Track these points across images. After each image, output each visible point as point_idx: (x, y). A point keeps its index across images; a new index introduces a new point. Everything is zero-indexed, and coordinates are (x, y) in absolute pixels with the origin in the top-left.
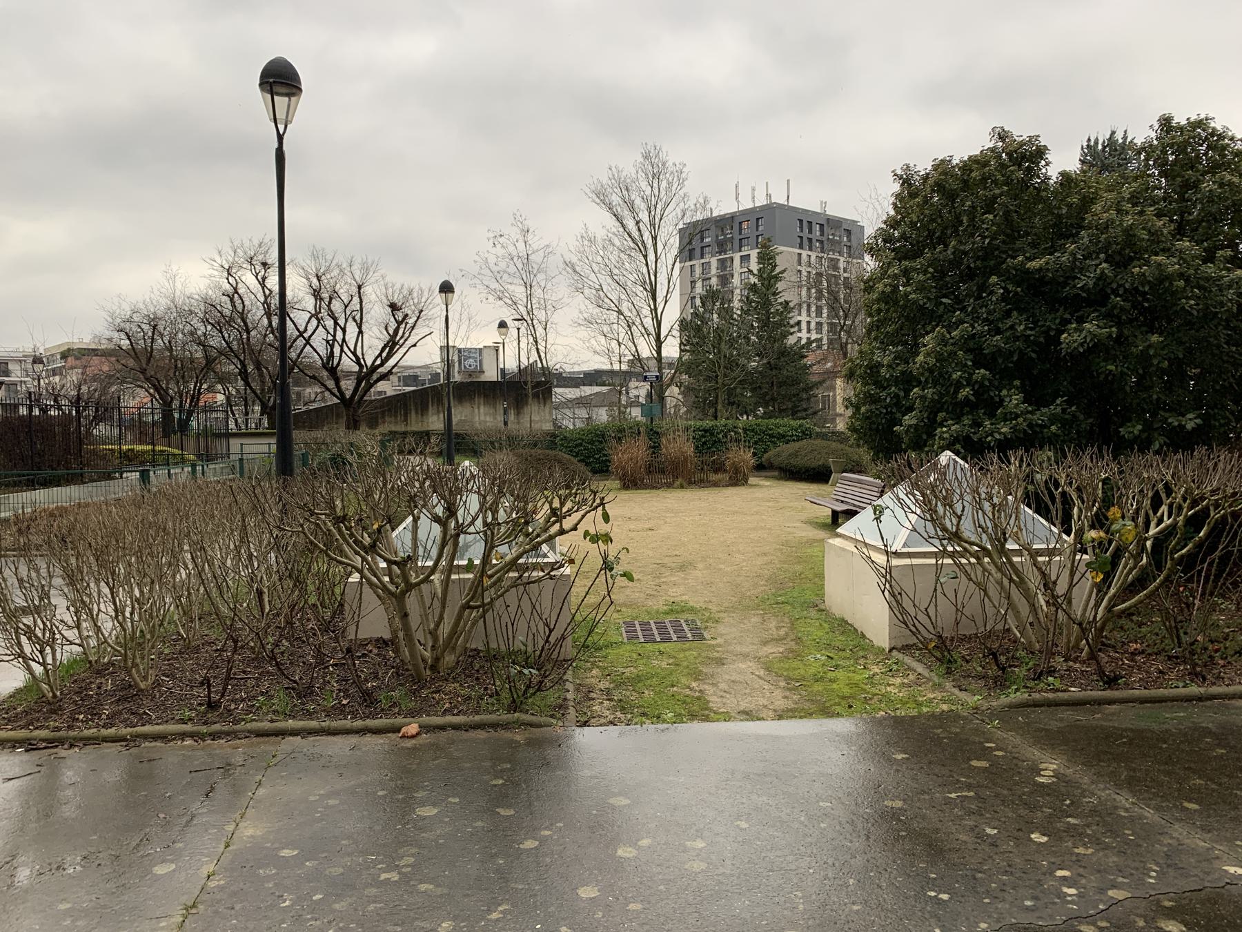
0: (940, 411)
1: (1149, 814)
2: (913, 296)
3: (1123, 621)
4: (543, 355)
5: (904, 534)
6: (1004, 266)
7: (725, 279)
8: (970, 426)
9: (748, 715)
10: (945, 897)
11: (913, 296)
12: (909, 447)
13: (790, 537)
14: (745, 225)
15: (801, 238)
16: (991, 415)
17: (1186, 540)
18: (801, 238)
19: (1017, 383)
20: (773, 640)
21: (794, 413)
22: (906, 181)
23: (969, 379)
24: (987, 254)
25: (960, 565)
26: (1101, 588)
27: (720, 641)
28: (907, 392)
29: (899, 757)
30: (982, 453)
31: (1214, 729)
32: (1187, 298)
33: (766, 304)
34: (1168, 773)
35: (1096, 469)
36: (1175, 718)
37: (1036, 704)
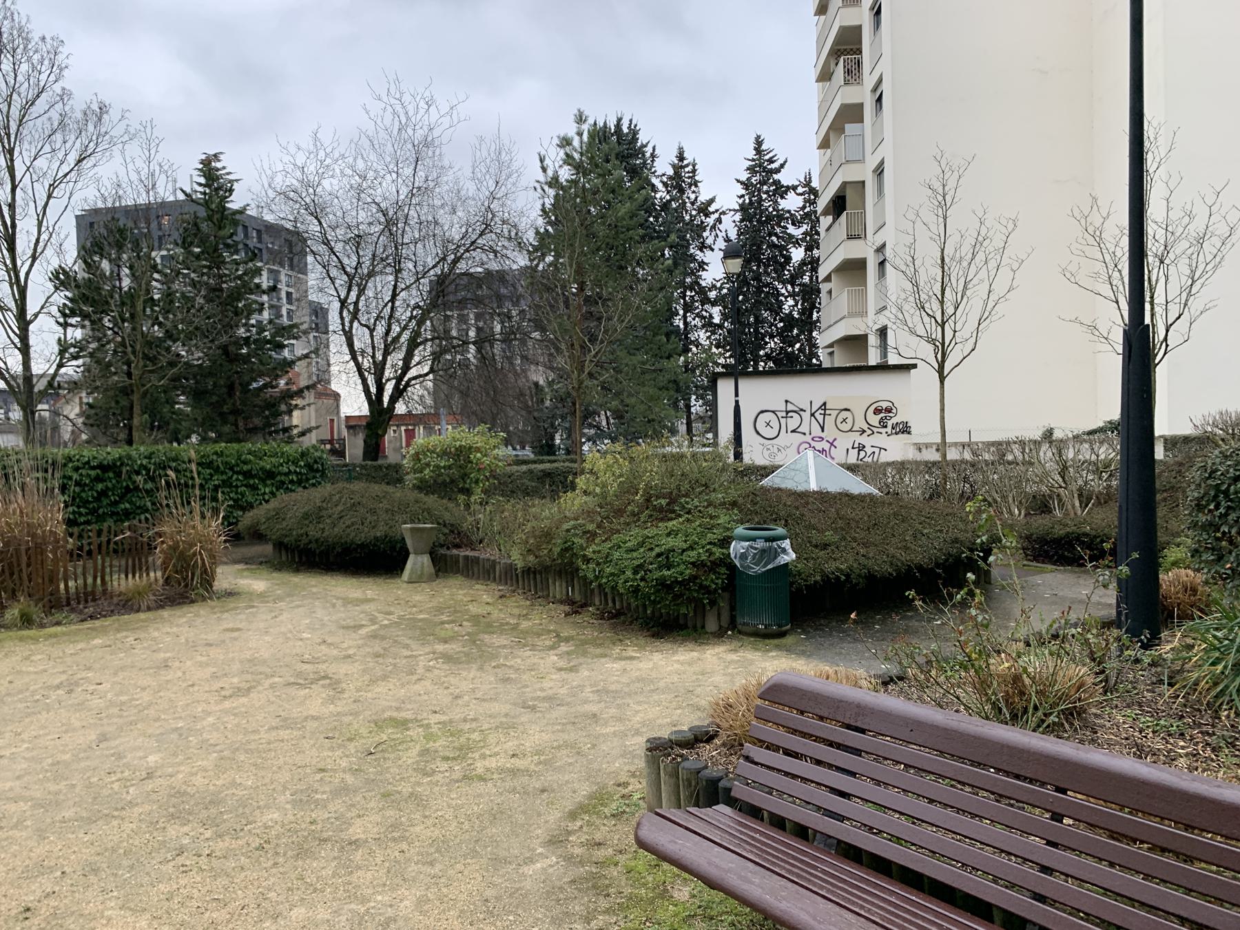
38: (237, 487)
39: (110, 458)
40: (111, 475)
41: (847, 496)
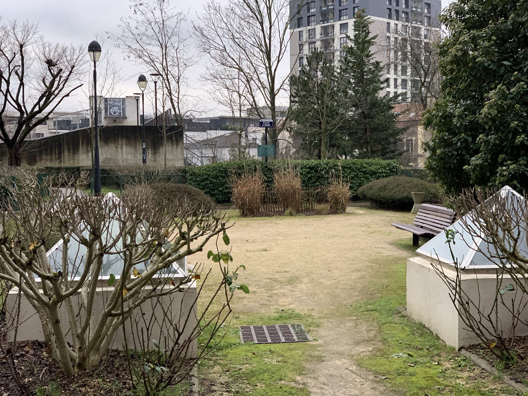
4: (176, 105)
5: (471, 254)
7: (327, 43)
11: (479, 59)
13: (379, 256)
15: (390, 9)
18: (390, 9)
20: (364, 341)
21: (384, 154)
25: (516, 280)
27: (320, 342)
28: (474, 137)
33: (360, 64)
38: (360, 178)
39: (313, 164)
40: (313, 171)
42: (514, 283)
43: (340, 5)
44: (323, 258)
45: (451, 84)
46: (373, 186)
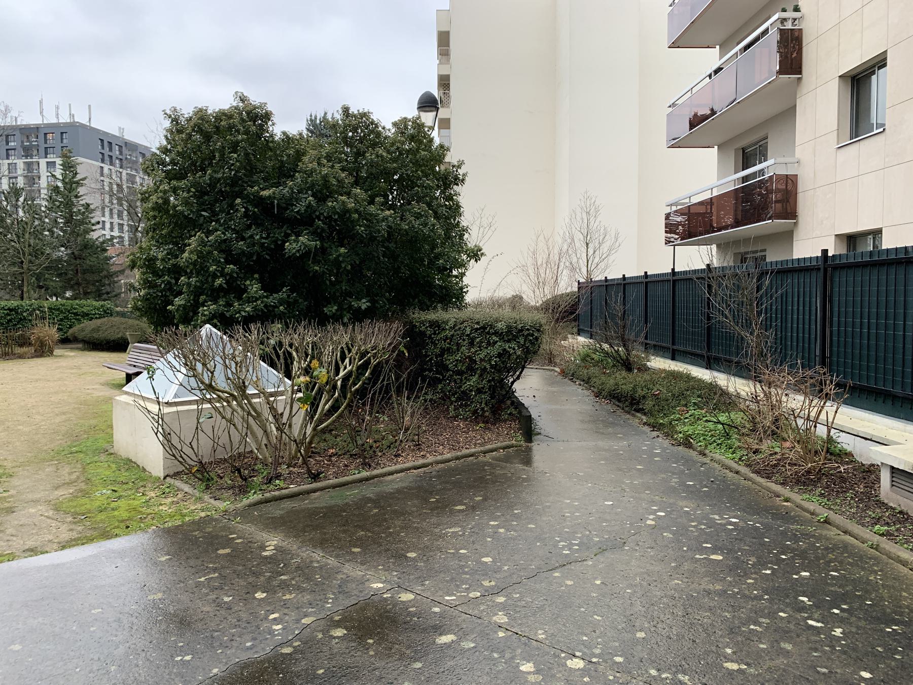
0: (201, 294)
1: (332, 561)
2: (179, 208)
3: (327, 436)
5: (174, 388)
6: (246, 192)
7: (32, 180)
8: (224, 306)
9: (33, 551)
10: (188, 658)
11: (179, 208)
12: (179, 322)
13: (88, 397)
14: (50, 136)
15: (103, 154)
16: (239, 298)
17: (358, 378)
18: (103, 154)
19: (256, 276)
20: (64, 484)
21: (99, 296)
22: (175, 121)
23: (221, 272)
24: (234, 182)
25: (216, 409)
26: (311, 415)
27: (12, 492)
28: (177, 280)
29: (163, 559)
30: (231, 325)
31: (374, 497)
32: (360, 226)
33: (69, 204)
34: (345, 532)
35: (308, 336)
36: (352, 494)
37: (267, 501)
41: (676, 281)
42: (213, 411)
43: (46, 143)
44: (22, 404)
45: (154, 229)
46: (85, 327)
